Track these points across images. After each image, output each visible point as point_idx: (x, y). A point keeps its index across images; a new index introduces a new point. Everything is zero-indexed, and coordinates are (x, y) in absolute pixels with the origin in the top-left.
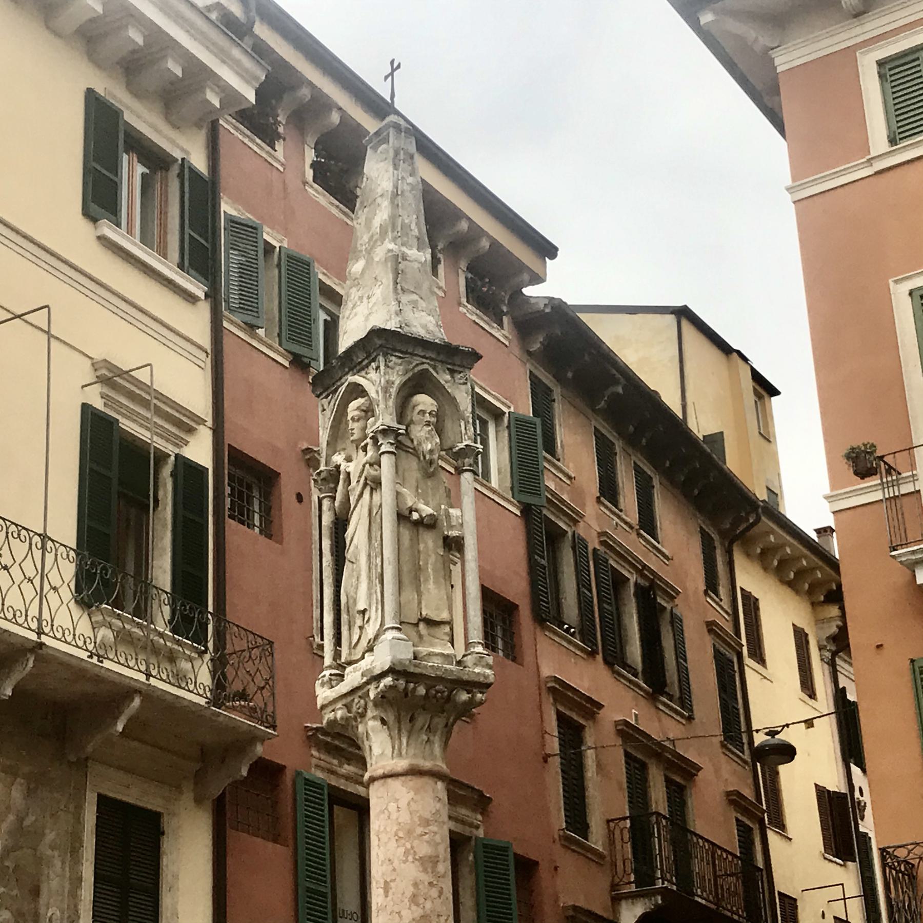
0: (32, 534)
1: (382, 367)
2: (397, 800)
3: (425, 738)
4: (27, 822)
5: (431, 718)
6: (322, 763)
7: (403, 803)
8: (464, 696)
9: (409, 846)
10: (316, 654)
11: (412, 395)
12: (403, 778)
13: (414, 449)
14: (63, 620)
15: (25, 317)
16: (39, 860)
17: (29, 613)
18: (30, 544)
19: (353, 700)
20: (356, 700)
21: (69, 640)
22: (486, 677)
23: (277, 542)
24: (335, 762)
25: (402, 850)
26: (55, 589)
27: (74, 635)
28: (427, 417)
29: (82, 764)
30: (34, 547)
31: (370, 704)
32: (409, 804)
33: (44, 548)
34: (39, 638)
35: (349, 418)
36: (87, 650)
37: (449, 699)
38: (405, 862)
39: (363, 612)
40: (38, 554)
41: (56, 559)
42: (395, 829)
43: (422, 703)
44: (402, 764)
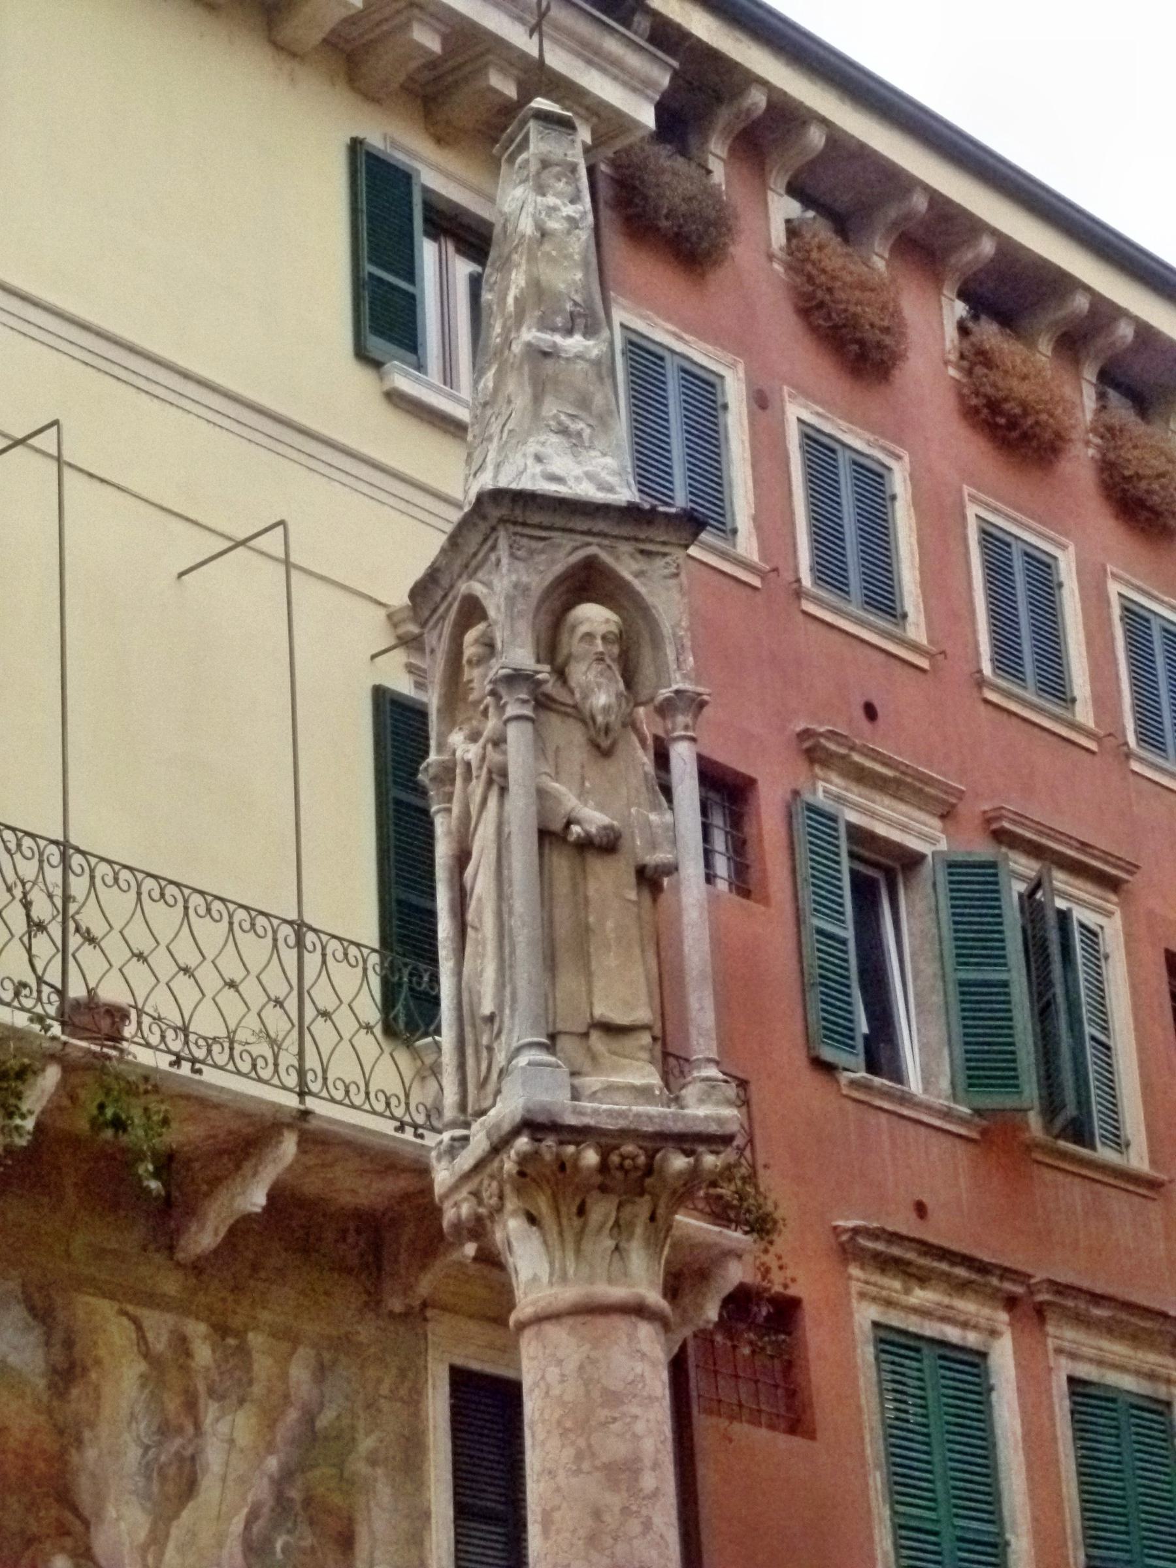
0: (275, 922)
1: (505, 561)
2: (560, 1362)
3: (610, 1243)
4: (323, 1421)
5: (620, 1206)
6: (872, 1290)
7: (571, 1366)
8: (679, 1162)
9: (581, 1442)
10: (846, 1096)
11: (568, 607)
12: (570, 1321)
13: (575, 707)
14: (343, 1068)
15: (252, 543)
16: (347, 1482)
17: (280, 1060)
18: (275, 940)
19: (481, 1183)
20: (486, 1182)
21: (357, 1102)
22: (720, 1121)
23: (757, 901)
24: (897, 1285)
25: (569, 1452)
26: (325, 1014)
27: (367, 1094)
28: (600, 646)
29: (416, 1316)
30: (281, 943)
31: (508, 1189)
32: (581, 1367)
33: (300, 944)
34: (302, 1101)
35: (464, 661)
36: (393, 1118)
37: (649, 1170)
38: (578, 1472)
39: (491, 1019)
40: (290, 957)
41: (324, 962)
42: (556, 1416)
43: (597, 1179)
44: (569, 1294)
